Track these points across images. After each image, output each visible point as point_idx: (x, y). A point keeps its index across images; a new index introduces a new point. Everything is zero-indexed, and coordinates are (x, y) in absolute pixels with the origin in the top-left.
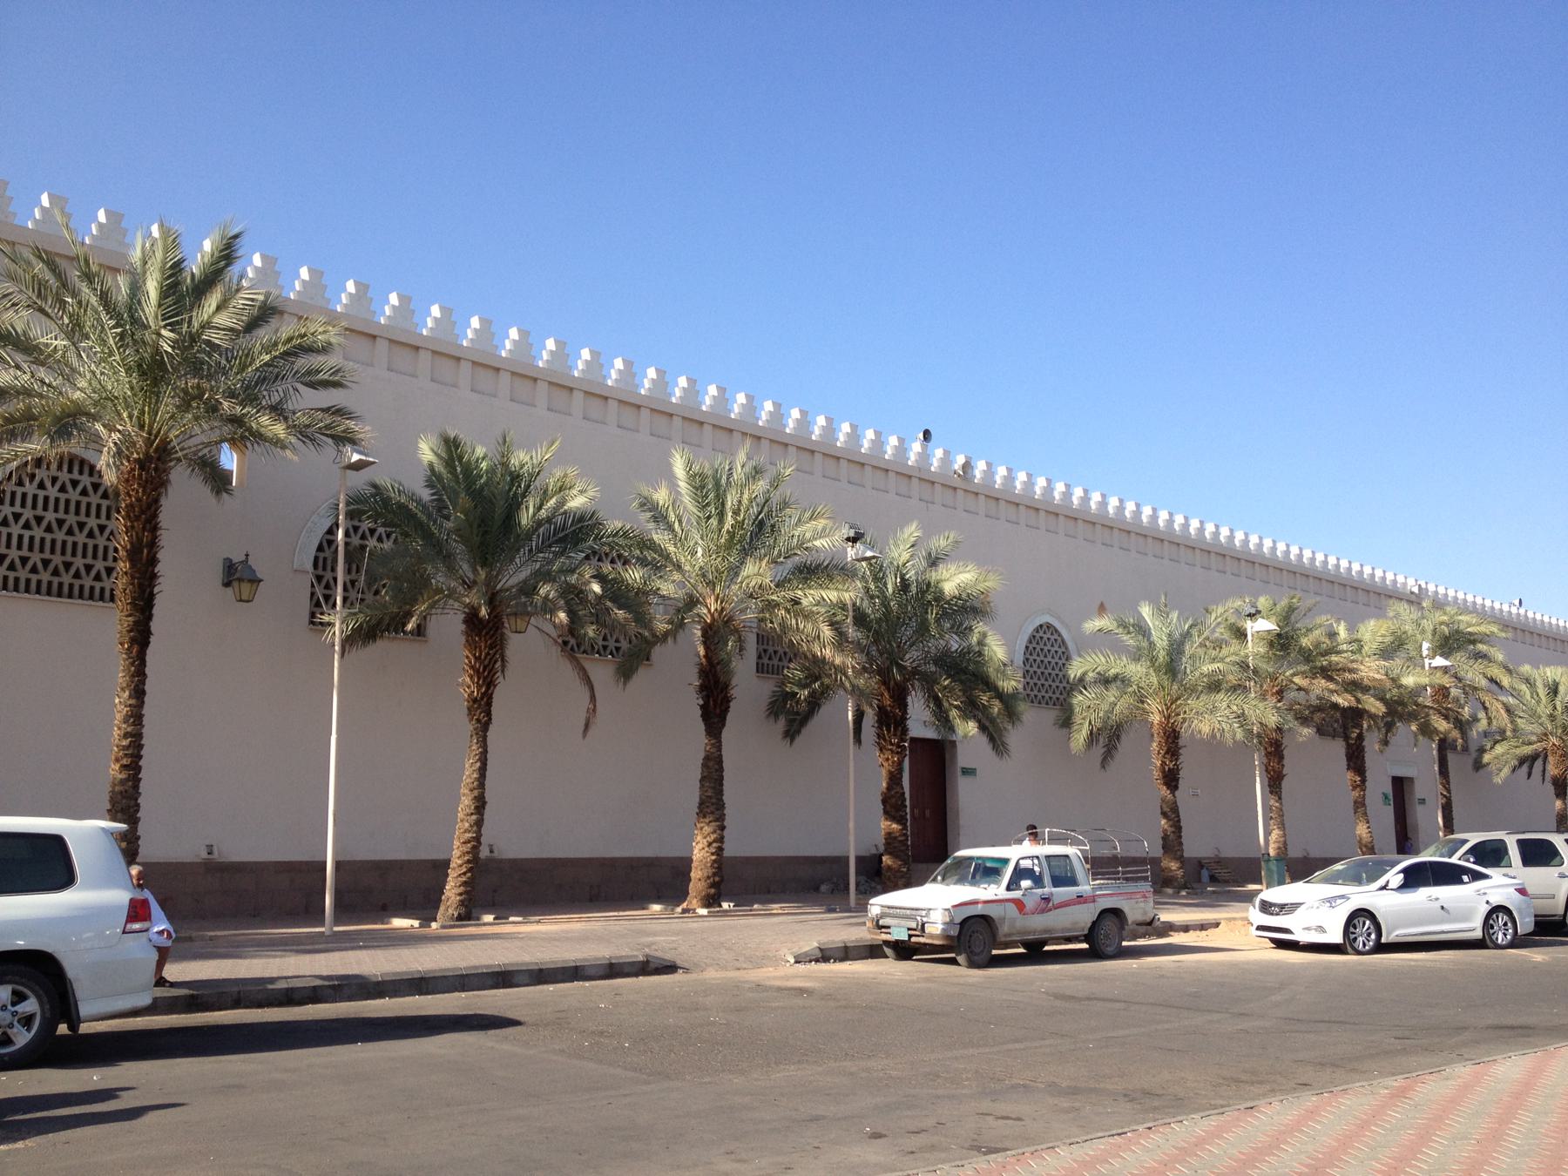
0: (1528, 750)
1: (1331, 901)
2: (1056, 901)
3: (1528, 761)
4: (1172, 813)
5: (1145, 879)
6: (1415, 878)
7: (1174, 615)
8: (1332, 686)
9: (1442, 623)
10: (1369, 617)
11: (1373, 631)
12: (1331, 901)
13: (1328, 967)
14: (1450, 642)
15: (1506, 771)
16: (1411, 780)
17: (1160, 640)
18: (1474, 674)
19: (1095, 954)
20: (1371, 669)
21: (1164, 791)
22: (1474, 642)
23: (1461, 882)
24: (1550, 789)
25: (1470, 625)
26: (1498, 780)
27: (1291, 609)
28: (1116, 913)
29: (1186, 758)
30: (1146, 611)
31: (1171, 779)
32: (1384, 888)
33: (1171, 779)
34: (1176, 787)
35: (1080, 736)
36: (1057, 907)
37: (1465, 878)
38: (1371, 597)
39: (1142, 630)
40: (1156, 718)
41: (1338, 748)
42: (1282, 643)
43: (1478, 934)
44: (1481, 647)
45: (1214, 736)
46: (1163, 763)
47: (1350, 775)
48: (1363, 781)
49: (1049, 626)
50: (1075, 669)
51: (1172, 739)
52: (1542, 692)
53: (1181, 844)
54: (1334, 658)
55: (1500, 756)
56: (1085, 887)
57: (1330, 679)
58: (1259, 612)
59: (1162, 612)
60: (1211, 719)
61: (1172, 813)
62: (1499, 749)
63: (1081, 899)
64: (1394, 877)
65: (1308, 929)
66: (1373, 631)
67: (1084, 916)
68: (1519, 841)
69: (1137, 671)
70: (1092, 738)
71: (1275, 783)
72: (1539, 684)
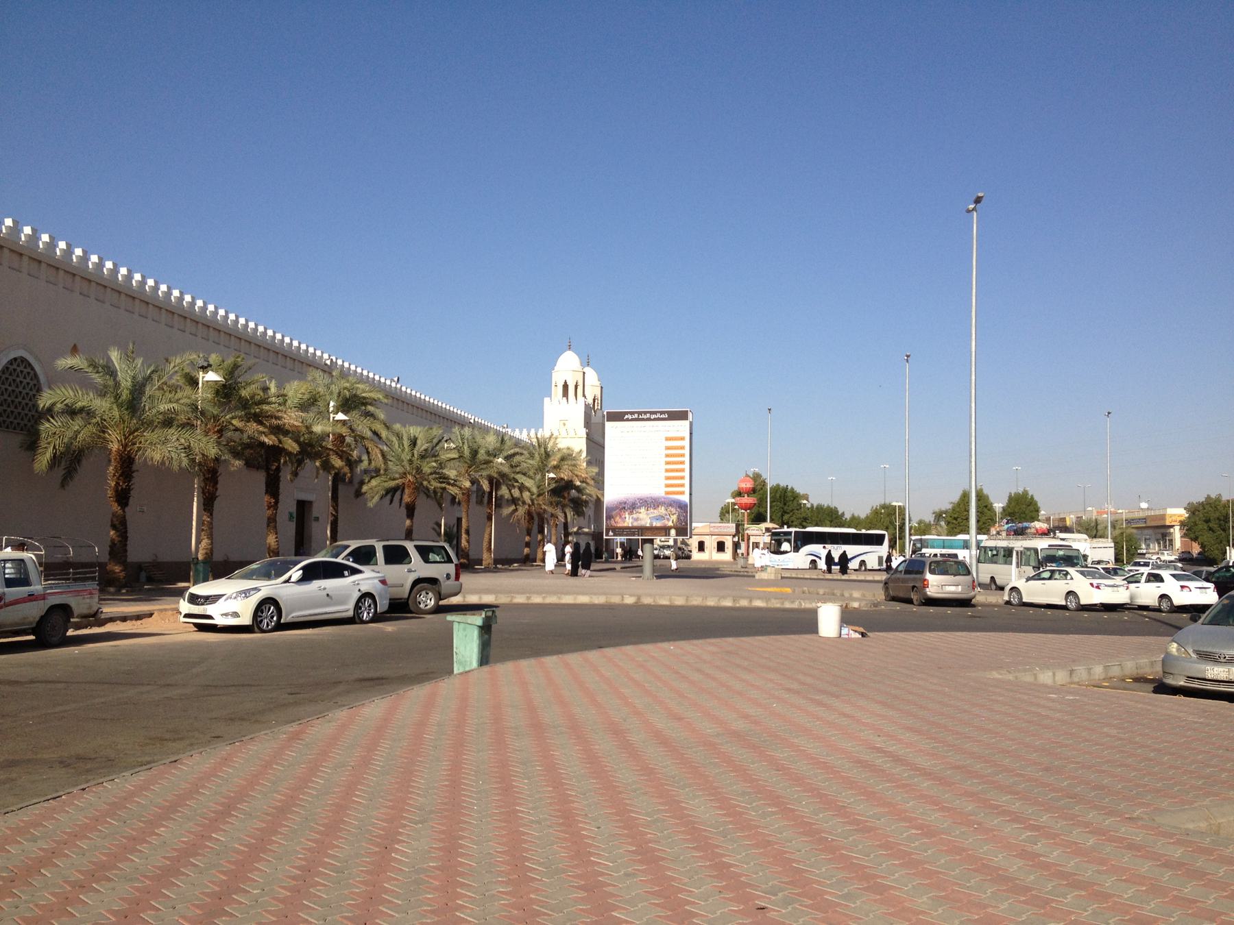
0: (392, 484)
1: (246, 593)
2: (8, 599)
3: (391, 492)
4: (120, 525)
5: (93, 579)
6: (311, 574)
7: (139, 361)
8: (261, 429)
9: (345, 388)
10: (294, 379)
11: (296, 390)
12: (246, 593)
13: (238, 643)
14: (349, 403)
15: (377, 498)
16: (310, 503)
17: (125, 380)
18: (363, 427)
19: (41, 644)
20: (292, 418)
21: (116, 507)
22: (365, 404)
23: (343, 576)
24: (404, 511)
25: (364, 392)
26: (371, 505)
27: (236, 366)
28: (65, 609)
29: (137, 480)
30: (114, 355)
31: (123, 497)
32: (287, 581)
33: (123, 497)
34: (126, 504)
35: (44, 459)
36: (7, 605)
37: (346, 573)
38: (298, 364)
39: (111, 372)
40: (115, 447)
41: (260, 478)
42: (225, 392)
43: (351, 613)
44: (370, 408)
45: (163, 463)
46: (117, 483)
47: (267, 498)
48: (277, 503)
49: (23, 360)
50: (45, 400)
51: (127, 464)
52: (406, 443)
53: (126, 551)
54: (265, 407)
55: (374, 487)
56: (37, 587)
57: (261, 423)
58: (210, 366)
59: (128, 357)
60: (163, 449)
61: (120, 525)
62: (374, 482)
63: (32, 597)
64: (296, 573)
65: (226, 615)
66: (296, 390)
67: (34, 611)
68: (385, 547)
69: (102, 405)
70: (55, 460)
71: (208, 504)
72: (405, 438)
